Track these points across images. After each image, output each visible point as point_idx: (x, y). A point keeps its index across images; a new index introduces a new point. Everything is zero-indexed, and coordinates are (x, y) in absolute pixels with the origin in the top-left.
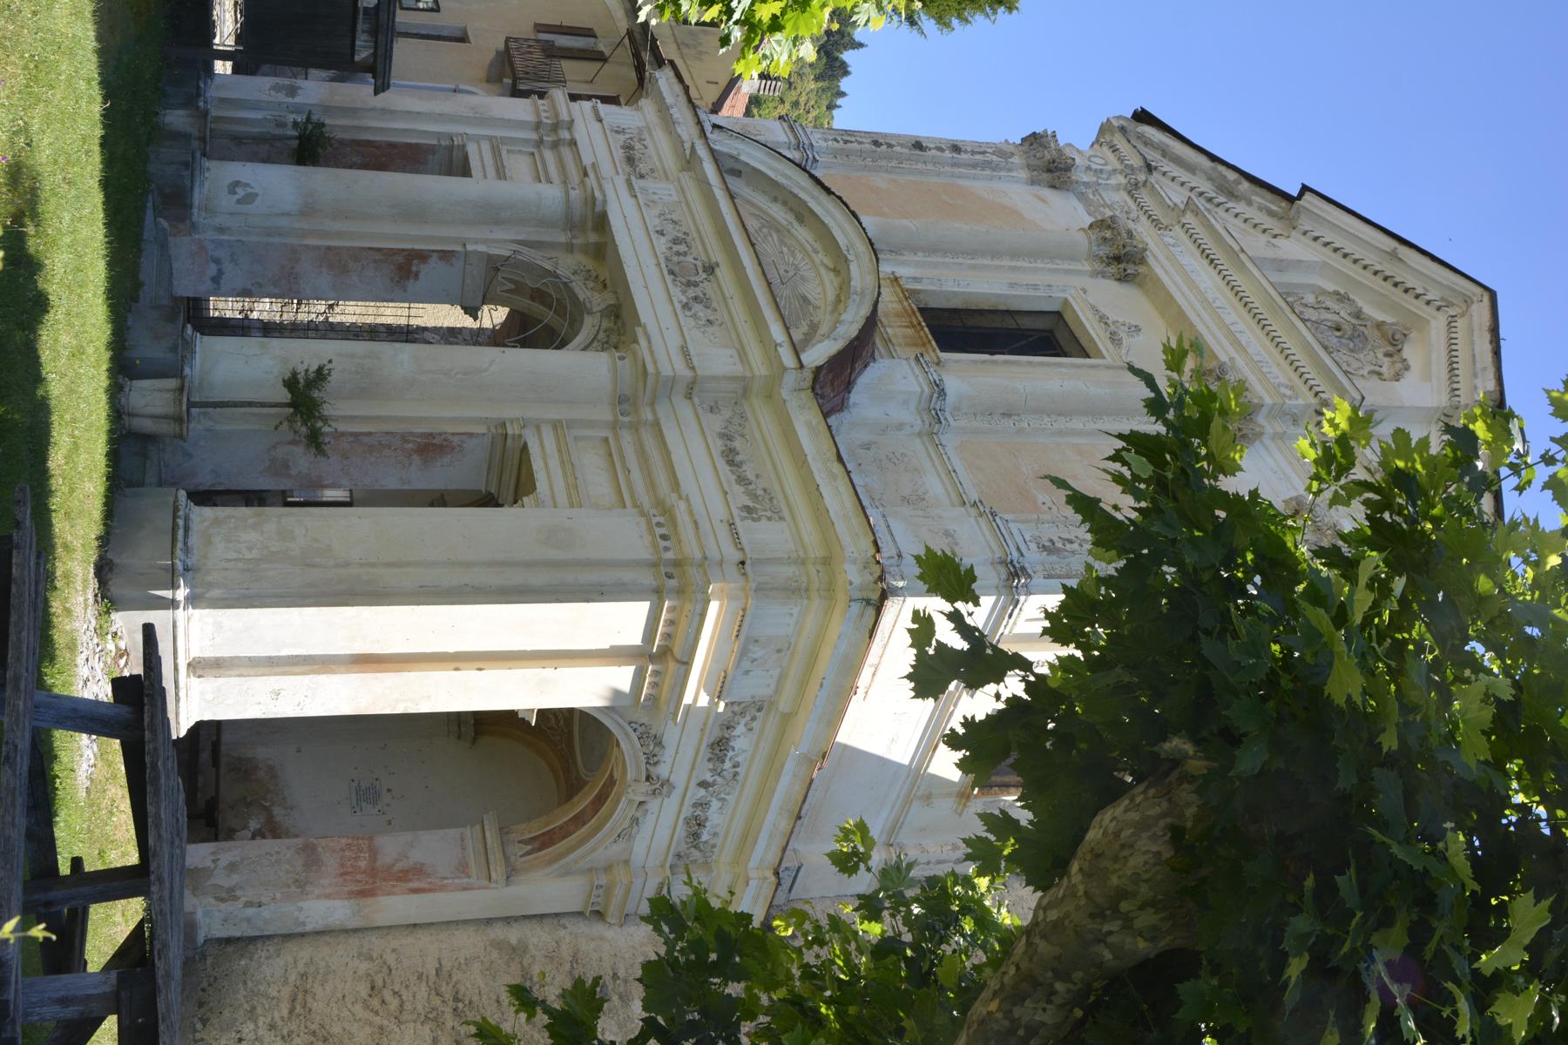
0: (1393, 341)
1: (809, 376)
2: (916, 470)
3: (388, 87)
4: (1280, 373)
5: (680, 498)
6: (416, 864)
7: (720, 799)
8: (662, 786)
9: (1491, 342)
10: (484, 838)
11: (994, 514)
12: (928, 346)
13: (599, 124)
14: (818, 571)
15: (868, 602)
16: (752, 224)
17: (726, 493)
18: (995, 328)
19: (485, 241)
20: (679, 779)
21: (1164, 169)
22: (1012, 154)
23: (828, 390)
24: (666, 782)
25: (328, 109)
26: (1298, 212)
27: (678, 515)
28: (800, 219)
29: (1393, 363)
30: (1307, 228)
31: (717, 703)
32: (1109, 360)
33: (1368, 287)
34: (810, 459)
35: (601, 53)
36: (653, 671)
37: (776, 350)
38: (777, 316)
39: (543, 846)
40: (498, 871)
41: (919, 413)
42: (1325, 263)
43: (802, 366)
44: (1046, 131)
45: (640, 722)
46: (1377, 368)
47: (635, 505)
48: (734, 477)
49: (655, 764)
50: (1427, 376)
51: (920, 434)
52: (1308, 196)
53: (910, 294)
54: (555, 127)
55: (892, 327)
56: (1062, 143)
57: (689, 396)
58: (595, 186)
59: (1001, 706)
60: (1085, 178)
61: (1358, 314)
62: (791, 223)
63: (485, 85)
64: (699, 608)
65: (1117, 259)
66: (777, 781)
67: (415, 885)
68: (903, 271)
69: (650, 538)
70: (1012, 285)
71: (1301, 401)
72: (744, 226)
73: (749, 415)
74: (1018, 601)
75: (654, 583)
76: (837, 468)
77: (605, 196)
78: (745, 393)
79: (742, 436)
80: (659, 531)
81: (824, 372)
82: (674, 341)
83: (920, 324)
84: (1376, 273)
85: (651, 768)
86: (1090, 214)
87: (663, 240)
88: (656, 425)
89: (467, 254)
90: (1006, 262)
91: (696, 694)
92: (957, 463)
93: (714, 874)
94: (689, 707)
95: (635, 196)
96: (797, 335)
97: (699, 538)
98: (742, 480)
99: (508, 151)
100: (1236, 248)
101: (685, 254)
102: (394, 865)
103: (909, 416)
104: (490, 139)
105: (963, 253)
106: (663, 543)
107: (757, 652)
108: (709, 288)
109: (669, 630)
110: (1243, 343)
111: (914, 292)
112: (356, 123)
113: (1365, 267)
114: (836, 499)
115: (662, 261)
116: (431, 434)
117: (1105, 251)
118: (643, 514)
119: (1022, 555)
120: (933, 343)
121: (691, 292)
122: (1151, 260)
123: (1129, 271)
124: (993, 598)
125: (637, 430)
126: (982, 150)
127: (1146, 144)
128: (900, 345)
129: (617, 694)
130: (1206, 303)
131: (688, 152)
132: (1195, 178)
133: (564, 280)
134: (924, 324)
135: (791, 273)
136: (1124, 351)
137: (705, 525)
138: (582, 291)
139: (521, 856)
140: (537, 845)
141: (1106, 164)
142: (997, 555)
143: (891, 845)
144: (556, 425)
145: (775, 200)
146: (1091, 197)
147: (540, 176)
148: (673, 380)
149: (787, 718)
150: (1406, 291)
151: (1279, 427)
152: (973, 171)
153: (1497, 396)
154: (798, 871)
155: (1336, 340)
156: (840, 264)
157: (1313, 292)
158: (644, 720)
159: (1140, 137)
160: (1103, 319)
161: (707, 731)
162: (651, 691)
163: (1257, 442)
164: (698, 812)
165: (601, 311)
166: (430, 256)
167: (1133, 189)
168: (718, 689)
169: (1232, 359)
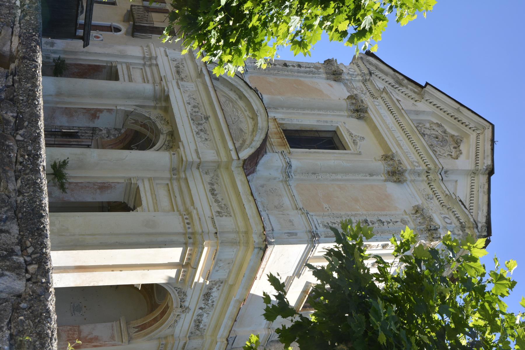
0: (457, 143)
1: (242, 162)
2: (280, 195)
3: (88, 45)
4: (414, 157)
5: (194, 209)
6: (95, 336)
7: (207, 313)
8: (186, 309)
9: (491, 145)
10: (121, 326)
11: (307, 213)
12: (286, 146)
13: (166, 57)
14: (243, 236)
15: (261, 249)
16: (222, 99)
17: (211, 206)
18: (312, 137)
19: (124, 105)
20: (192, 306)
21: (376, 74)
22: (320, 68)
23: (248, 167)
24: (188, 308)
25: (65, 52)
26: (424, 92)
27: (193, 215)
28: (240, 98)
29: (456, 151)
30: (427, 98)
31: (206, 282)
32: (352, 151)
33: (448, 121)
34: (241, 194)
35: (168, 10)
36: (183, 271)
37: (230, 152)
38: (231, 139)
39: (142, 329)
40: (125, 338)
41: (282, 173)
42: (434, 112)
43: (239, 159)
44: (333, 58)
45: (178, 287)
46: (450, 153)
47: (178, 211)
48: (214, 200)
49: (184, 302)
50: (468, 158)
51: (282, 181)
52: (428, 87)
53: (280, 125)
54: (151, 59)
55: (273, 138)
56: (338, 63)
57: (198, 168)
58: (165, 85)
59: (293, 324)
60: (347, 78)
61: (445, 132)
62: (237, 99)
63: (123, 23)
64: (200, 250)
65: (357, 111)
66: (228, 308)
67: (95, 344)
68: (278, 116)
69: (183, 224)
70: (318, 121)
71: (421, 168)
72: (219, 102)
73: (220, 175)
74: (315, 246)
75: (184, 241)
76: (251, 198)
77: (168, 89)
78: (219, 167)
79: (217, 184)
80: (186, 221)
81: (247, 161)
82: (193, 147)
83: (283, 137)
84: (452, 116)
85: (182, 303)
86: (348, 92)
87: (190, 106)
88: (186, 179)
89: (117, 110)
90: (316, 112)
91: (199, 278)
92: (295, 193)
93: (205, 339)
94: (196, 283)
95: (180, 89)
96: (238, 145)
97: (200, 224)
98: (217, 201)
99: (133, 68)
100: (400, 108)
101: (198, 112)
102: (87, 337)
103: (278, 175)
104: (126, 63)
105: (300, 108)
106: (187, 226)
107: (221, 264)
108: (206, 126)
109: (189, 257)
110: (401, 145)
111: (281, 124)
112: (77, 57)
113: (448, 114)
114: (250, 210)
115: (189, 115)
116: (104, 183)
117: (353, 107)
118: (181, 215)
119: (317, 229)
120: (288, 145)
121: (200, 127)
122: (369, 112)
123: (361, 116)
124: (306, 245)
125: (179, 181)
126: (309, 66)
127: (370, 64)
128: (276, 146)
129: (170, 278)
130: (388, 129)
131: (199, 70)
132: (387, 77)
133: (154, 121)
134: (285, 137)
135: (236, 119)
136: (358, 147)
137: (203, 219)
138: (160, 125)
139: (134, 333)
140: (140, 329)
141: (355, 72)
142: (308, 229)
143: (270, 328)
144: (150, 179)
145: (231, 90)
146: (349, 84)
147: (145, 80)
148: (193, 163)
149: (231, 286)
150: (462, 123)
151: (413, 177)
152: (306, 75)
153: (491, 167)
154: (235, 338)
155: (436, 142)
156: (254, 117)
157: (429, 123)
158: (180, 287)
159: (368, 61)
160: (351, 135)
161: (203, 291)
162: (182, 278)
163: (405, 183)
164: (199, 318)
165: (166, 133)
166: (103, 111)
167: (364, 81)
168: (207, 277)
169: (397, 152)
